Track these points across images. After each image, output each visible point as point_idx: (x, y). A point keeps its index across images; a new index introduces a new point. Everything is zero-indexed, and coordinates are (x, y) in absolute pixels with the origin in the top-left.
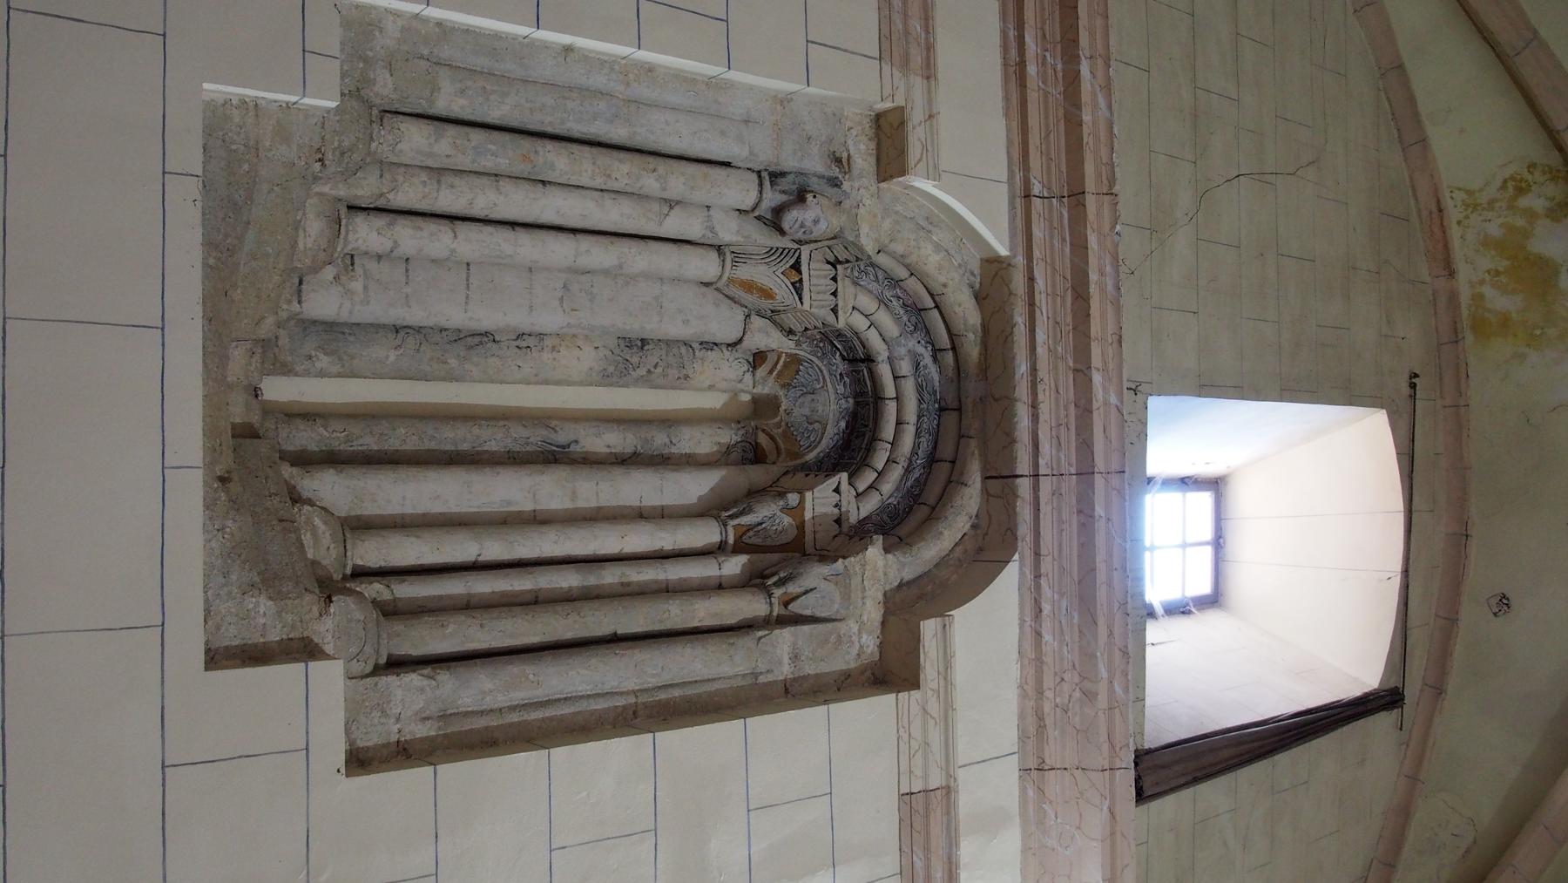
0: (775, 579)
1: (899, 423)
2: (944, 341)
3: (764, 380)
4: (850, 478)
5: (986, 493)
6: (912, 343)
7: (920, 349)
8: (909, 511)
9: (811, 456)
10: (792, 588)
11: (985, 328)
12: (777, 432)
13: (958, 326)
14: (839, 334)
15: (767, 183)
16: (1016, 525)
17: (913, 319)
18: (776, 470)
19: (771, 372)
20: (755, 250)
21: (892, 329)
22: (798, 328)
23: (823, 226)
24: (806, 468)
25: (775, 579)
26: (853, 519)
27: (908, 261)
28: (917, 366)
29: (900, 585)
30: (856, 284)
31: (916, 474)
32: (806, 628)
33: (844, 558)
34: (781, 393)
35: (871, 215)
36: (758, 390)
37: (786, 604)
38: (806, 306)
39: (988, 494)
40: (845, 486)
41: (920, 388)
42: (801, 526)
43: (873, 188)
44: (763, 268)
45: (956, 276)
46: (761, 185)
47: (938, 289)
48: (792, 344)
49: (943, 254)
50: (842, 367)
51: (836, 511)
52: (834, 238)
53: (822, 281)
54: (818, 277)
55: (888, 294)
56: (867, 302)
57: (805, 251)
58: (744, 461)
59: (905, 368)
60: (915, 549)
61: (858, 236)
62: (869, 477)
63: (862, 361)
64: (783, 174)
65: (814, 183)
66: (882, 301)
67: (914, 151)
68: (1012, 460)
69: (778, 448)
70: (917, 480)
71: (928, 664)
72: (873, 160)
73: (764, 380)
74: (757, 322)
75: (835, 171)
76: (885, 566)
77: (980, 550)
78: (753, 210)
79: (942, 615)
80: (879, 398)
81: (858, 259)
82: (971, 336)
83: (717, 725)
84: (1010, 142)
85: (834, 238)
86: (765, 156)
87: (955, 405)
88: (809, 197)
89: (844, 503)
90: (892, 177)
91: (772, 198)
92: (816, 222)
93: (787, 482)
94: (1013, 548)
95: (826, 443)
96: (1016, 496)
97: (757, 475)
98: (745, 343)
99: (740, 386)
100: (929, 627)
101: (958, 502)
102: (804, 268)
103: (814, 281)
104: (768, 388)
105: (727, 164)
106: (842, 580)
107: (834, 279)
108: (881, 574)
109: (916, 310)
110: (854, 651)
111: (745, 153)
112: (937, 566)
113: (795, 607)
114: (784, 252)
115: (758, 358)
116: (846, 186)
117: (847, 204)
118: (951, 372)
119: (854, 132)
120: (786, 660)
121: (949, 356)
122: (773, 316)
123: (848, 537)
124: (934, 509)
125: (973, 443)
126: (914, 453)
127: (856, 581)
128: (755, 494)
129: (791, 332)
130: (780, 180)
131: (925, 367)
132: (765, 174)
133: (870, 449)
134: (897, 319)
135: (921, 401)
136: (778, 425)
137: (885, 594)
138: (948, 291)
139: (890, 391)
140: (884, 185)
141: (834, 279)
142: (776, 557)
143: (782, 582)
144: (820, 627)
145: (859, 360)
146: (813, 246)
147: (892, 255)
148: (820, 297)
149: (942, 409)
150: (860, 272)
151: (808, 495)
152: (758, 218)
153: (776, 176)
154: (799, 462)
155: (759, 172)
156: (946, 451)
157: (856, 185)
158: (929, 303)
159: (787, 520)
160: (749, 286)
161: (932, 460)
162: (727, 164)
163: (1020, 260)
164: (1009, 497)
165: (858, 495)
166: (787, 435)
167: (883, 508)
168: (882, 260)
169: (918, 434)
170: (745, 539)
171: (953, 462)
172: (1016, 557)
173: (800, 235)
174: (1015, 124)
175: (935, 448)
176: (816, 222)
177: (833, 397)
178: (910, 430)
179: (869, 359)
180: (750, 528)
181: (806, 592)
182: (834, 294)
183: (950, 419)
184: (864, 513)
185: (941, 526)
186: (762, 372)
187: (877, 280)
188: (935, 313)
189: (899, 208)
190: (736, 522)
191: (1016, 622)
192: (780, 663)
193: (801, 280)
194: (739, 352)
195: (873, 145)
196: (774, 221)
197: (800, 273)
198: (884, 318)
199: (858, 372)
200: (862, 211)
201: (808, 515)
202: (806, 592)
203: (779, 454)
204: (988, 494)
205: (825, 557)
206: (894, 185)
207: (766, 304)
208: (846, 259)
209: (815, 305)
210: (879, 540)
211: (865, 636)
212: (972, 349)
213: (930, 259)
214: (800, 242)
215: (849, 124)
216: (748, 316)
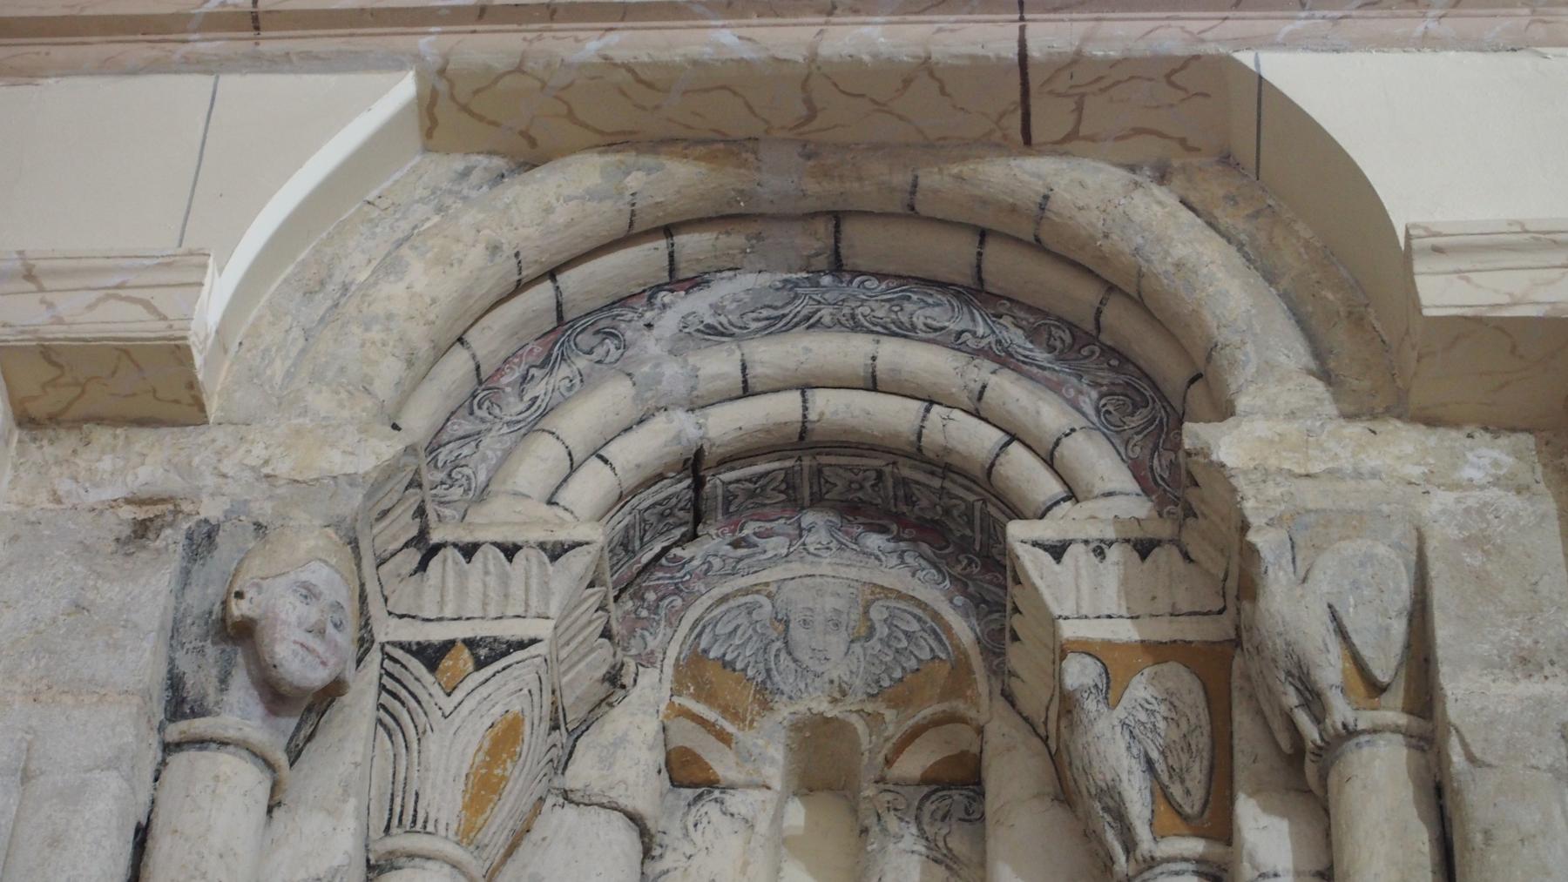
0: (1303, 720)
1: (872, 384)
2: (645, 258)
3: (746, 757)
4: (1020, 515)
5: (1067, 143)
6: (651, 346)
7: (668, 323)
8: (1118, 357)
9: (964, 630)
10: (1330, 670)
11: (613, 142)
12: (894, 723)
13: (607, 217)
14: (624, 545)
15: (199, 726)
16: (1156, 60)
17: (585, 340)
18: (1001, 728)
19: (724, 738)
20: (383, 766)
21: (610, 398)
22: (603, 657)
23: (319, 575)
24: (996, 643)
25: (1303, 720)
26: (1141, 508)
27: (424, 349)
28: (714, 332)
29: (1325, 375)
30: (483, 494)
31: (1015, 337)
32: (1444, 632)
33: (1244, 527)
34: (784, 712)
35: (295, 443)
36: (775, 774)
37: (1376, 689)
38: (543, 629)
39: (1073, 136)
40: (1046, 530)
41: (776, 325)
42: (1157, 651)
43: (221, 436)
44: (433, 744)
45: (471, 217)
46: (201, 743)
47: (503, 272)
48: (648, 677)
49: (405, 250)
50: (713, 543)
51: (1114, 554)
52: (354, 544)
53: (474, 585)
54: (462, 590)
55: (513, 407)
56: (537, 463)
57: (388, 630)
58: (975, 818)
59: (719, 364)
60: (1222, 336)
61: (351, 479)
62: (1022, 468)
63: (698, 484)
64: (175, 683)
65: (203, 597)
66: (537, 421)
67: (124, 320)
68: (978, 68)
69: (936, 722)
70: (1032, 334)
71: (1543, 295)
72: (144, 438)
73: (746, 757)
74: (584, 772)
75: (172, 538)
76: (1267, 416)
77: (1227, 160)
78: (269, 765)
79: (1407, 257)
80: (803, 440)
81: (415, 483)
82: (635, 181)
83: (1335, 136)
84: (106, 68)
85: (354, 544)
86: (125, 727)
87: (823, 228)
88: (239, 609)
89: (1093, 532)
90: (192, 385)
91: (239, 713)
92: (309, 593)
93: (1034, 695)
94: (1224, 67)
95: (932, 591)
96: (1077, 59)
97: (1012, 776)
98: (642, 803)
99: (763, 826)
100: (1441, 292)
101: (1091, 220)
102: (436, 634)
103: (473, 607)
104: (767, 749)
105: (142, 835)
106: (1309, 532)
107: (469, 551)
108: (1293, 429)
109: (562, 327)
110: (1511, 501)
111: (112, 782)
112: (1270, 278)
113: (1384, 665)
114: (391, 688)
115: (686, 773)
116: (211, 510)
117: (264, 509)
118: (736, 240)
119: (64, 486)
120: (1534, 688)
121: (692, 244)
122: (568, 728)
123: (1186, 512)
124: (1111, 288)
125: (935, 178)
126: (956, 342)
127: (1311, 496)
128: (1067, 786)
129: (614, 679)
130: (191, 693)
131: (717, 309)
132: (174, 731)
133: (945, 466)
134: (584, 383)
135: (811, 323)
136: (874, 720)
137: (1350, 417)
138: (509, 239)
139: (782, 408)
140: (213, 408)
141: (469, 551)
142: (1242, 720)
143: (1313, 699)
144: (1440, 594)
145: (697, 493)
146: (376, 608)
147: (407, 392)
148: (517, 589)
149: (837, 266)
150: (450, 481)
151: (1069, 630)
152: (295, 755)
153: (179, 702)
154: (976, 661)
155: (169, 748)
156: (951, 254)
157: (210, 481)
158: (542, 294)
159: (1140, 689)
160: (483, 788)
161: (975, 292)
162: (142, 835)
163: (429, 43)
164: (1085, 80)
165: (1072, 496)
166: (900, 695)
167: (1109, 425)
168: (420, 419)
169: (904, 332)
170: (1191, 807)
171: (983, 235)
172: (1246, 58)
173: (346, 640)
174: (60, 53)
175: (943, 286)
176: (309, 593)
177: (797, 568)
178: (895, 354)
179: (695, 465)
180: (1161, 793)
181: (1342, 633)
182: (510, 551)
183: (863, 241)
184: (1124, 480)
185: (1160, 265)
186: (723, 765)
187: (474, 437)
188: (568, 279)
189: (278, 368)
190: (1143, 832)
191: (1427, 58)
192: (1541, 703)
193: (471, 643)
194: (668, 825)
195: (102, 436)
196: (306, 708)
197: (448, 645)
198: (582, 419)
199: (729, 499)
200: (283, 468)
201: (1126, 632)
202: (1342, 633)
203: (952, 718)
204: (1073, 136)
205: (1241, 582)
206: (217, 382)
207: (535, 742)
208: (415, 519)
209: (540, 606)
210: (1195, 433)
211: (1468, 473)
212: (674, 179)
213: (423, 287)
214: (365, 643)
215: (42, 499)
216: (567, 796)
